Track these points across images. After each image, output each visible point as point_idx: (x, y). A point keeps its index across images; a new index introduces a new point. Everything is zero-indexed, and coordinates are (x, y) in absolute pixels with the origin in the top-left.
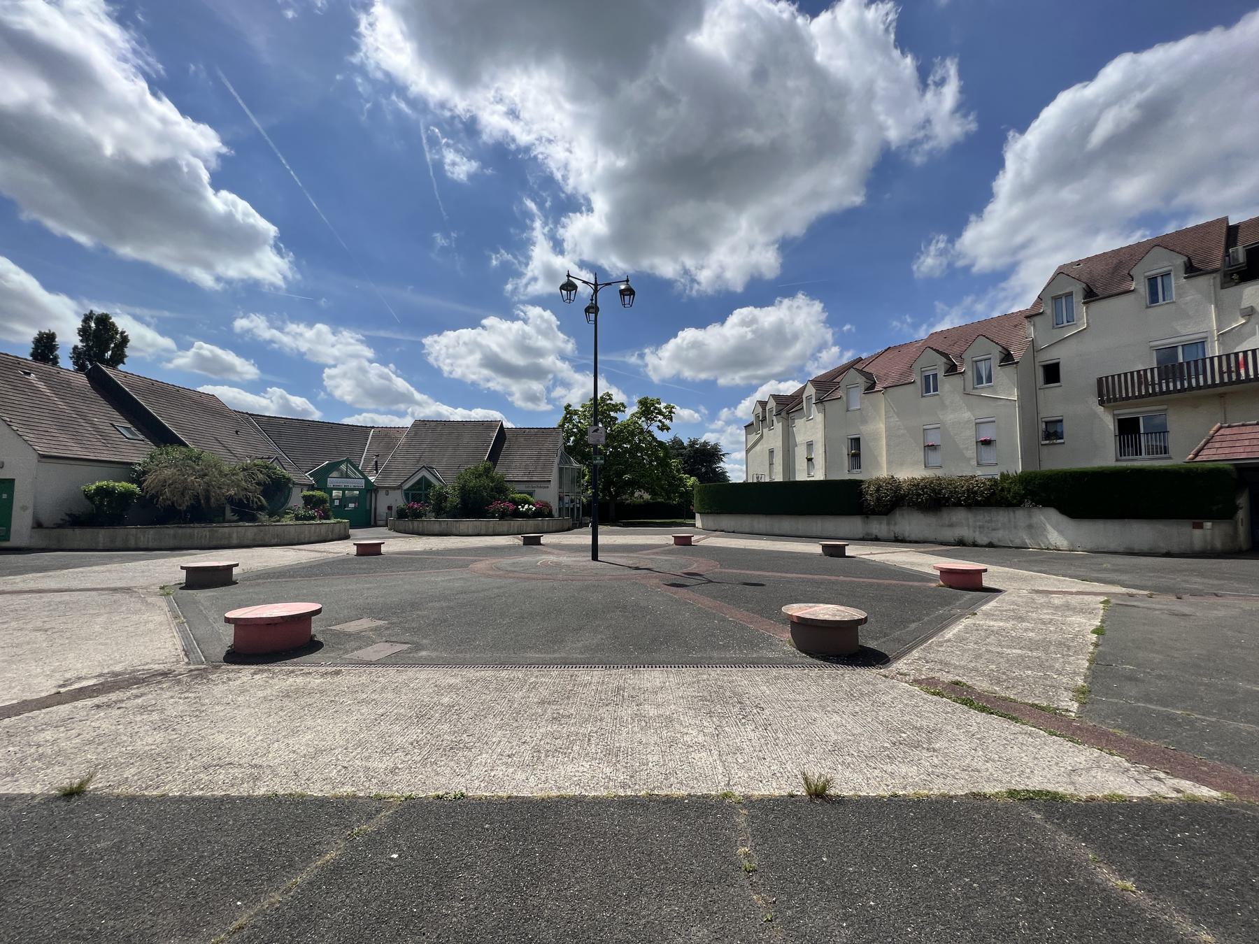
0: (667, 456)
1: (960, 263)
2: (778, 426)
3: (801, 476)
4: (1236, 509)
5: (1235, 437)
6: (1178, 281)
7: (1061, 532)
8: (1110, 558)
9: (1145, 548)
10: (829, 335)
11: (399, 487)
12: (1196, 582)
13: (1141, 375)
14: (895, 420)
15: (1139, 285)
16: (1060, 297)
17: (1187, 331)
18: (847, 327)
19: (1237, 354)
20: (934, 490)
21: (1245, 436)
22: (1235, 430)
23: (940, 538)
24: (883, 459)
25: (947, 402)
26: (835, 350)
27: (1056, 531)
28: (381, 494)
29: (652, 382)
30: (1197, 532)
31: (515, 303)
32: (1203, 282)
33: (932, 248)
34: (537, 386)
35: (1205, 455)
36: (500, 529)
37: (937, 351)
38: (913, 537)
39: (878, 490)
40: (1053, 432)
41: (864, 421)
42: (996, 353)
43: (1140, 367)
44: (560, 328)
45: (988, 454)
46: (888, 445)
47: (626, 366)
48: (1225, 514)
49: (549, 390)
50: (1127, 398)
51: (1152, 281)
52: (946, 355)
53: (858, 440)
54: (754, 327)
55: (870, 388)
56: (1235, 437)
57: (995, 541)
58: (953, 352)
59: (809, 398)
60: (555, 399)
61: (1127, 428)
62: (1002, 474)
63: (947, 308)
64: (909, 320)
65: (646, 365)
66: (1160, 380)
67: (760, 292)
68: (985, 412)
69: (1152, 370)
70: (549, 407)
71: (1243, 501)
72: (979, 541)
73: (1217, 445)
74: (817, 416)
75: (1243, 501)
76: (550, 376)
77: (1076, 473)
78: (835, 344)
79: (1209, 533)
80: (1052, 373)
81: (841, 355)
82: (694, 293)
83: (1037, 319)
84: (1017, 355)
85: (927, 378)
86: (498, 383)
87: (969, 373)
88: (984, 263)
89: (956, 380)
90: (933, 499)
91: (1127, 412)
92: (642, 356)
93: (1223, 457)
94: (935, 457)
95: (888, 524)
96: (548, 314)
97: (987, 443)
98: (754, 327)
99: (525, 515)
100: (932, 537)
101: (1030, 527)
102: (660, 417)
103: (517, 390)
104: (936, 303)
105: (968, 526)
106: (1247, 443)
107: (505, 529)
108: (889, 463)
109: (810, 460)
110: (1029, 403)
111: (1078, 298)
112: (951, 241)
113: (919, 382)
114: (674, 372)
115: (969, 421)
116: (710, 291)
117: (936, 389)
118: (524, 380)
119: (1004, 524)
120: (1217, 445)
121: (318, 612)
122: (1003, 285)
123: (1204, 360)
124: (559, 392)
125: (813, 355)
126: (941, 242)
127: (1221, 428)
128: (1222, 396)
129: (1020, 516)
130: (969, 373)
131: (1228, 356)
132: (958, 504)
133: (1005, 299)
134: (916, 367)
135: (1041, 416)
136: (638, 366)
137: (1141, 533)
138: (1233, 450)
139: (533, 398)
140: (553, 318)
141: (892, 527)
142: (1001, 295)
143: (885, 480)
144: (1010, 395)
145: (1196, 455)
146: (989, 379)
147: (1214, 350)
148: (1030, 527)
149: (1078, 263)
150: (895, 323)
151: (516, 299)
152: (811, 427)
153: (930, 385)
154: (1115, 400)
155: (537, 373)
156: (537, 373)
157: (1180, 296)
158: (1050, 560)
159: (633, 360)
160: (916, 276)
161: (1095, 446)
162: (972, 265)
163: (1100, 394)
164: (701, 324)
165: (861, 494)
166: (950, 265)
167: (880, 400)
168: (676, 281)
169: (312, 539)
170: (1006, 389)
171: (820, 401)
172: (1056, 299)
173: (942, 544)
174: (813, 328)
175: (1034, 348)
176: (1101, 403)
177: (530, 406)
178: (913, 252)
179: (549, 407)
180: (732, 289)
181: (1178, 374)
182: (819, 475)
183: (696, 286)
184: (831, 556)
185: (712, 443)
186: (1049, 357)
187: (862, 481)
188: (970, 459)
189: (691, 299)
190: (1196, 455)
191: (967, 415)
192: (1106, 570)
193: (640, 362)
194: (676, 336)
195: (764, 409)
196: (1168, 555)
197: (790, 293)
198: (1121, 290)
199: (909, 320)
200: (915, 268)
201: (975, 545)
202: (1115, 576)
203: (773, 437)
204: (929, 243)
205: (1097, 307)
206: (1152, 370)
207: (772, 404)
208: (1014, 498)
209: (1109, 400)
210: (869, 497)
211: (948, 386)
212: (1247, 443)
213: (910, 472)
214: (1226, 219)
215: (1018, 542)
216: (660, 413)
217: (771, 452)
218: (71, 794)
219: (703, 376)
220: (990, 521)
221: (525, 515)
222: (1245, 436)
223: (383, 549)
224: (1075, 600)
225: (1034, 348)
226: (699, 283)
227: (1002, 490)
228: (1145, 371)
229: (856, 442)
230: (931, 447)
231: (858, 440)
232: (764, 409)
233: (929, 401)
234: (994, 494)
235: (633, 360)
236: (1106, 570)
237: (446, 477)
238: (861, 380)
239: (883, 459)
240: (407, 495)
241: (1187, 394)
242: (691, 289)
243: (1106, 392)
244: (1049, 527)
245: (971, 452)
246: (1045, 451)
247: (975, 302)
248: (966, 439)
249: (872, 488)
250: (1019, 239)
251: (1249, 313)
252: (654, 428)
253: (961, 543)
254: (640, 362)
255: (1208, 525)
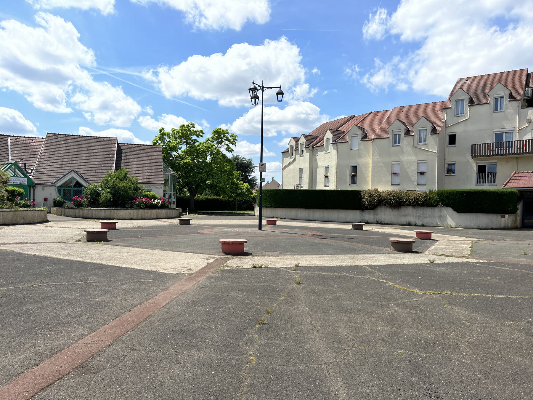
0: (232, 169)
1: (394, 31)
2: (307, 155)
3: (320, 186)
4: (517, 209)
5: (520, 178)
6: (506, 101)
7: (453, 219)
8: (471, 230)
9: (484, 227)
10: (302, 74)
11: (53, 185)
12: (499, 237)
13: (489, 145)
14: (377, 157)
15: (490, 100)
16: (459, 100)
17: (507, 126)
18: (315, 71)
19: (523, 141)
20: (398, 198)
21: (523, 178)
22: (520, 175)
23: (399, 222)
24: (370, 179)
25: (405, 150)
26: (306, 86)
27: (450, 217)
28: (38, 189)
29: (165, 97)
30: (503, 219)
31: (36, 11)
32: (516, 104)
33: (377, 17)
34: (57, 91)
35: (510, 185)
36: (145, 216)
37: (400, 121)
38: (386, 222)
39: (370, 196)
40: (450, 170)
41: (360, 156)
42: (429, 129)
43: (489, 142)
44: (80, 40)
45: (422, 178)
46: (372, 171)
47: (141, 80)
48: (513, 212)
49: (68, 95)
50: (483, 156)
51: (496, 99)
52: (404, 123)
53: (356, 167)
54: (248, 60)
55: (364, 138)
56: (520, 178)
57: (425, 224)
58: (408, 121)
59: (328, 140)
60: (75, 104)
61: (481, 169)
62: (430, 191)
63: (381, 64)
64: (357, 69)
65: (160, 82)
66: (496, 148)
67: (253, 33)
68: (422, 157)
69: (493, 143)
70: (69, 110)
71: (520, 206)
72: (418, 224)
73: (513, 181)
74: (333, 151)
75: (520, 206)
76: (70, 82)
77: (461, 191)
78: (306, 82)
79: (507, 220)
80: (452, 139)
81: (310, 91)
82: (202, 26)
83: (448, 110)
84: (439, 130)
85: (395, 135)
86: (17, 84)
87: (416, 136)
88: (407, 35)
89: (409, 139)
90: (397, 202)
91: (482, 162)
92: (156, 74)
93: (515, 186)
94: (397, 180)
95: (374, 214)
96: (69, 26)
97: (422, 173)
98: (248, 60)
99: (155, 207)
100: (395, 222)
101: (440, 216)
102: (227, 142)
103: (37, 93)
104: (375, 59)
105: (413, 216)
106: (523, 180)
107: (149, 216)
108: (373, 181)
109: (326, 177)
110: (442, 154)
111: (466, 103)
112: (390, 14)
113: (391, 138)
114: (183, 90)
115: (415, 161)
116: (215, 27)
117: (399, 143)
118: (43, 83)
119: (430, 215)
120: (513, 181)
121: (246, 242)
122: (418, 52)
123: (512, 142)
124: (78, 97)
125: (290, 88)
126: (382, 13)
127: (515, 173)
128: (517, 158)
129: (436, 211)
130: (416, 136)
131: (520, 141)
132: (409, 205)
133: (418, 61)
134: (390, 129)
135: (446, 161)
136: (153, 82)
137: (483, 219)
138: (519, 183)
139: (53, 101)
140: (75, 31)
141: (376, 216)
142: (417, 58)
143: (373, 191)
144: (434, 149)
145: (506, 185)
146: (425, 141)
147: (516, 138)
148: (440, 216)
149: (467, 79)
150: (348, 70)
151: (37, 6)
152: (328, 157)
153: (396, 141)
154: (478, 156)
155: (57, 78)
156: (57, 78)
157: (506, 109)
158: (449, 230)
159: (148, 75)
160: (364, 36)
161: (467, 181)
162: (401, 34)
163: (472, 153)
164: (207, 53)
165: (361, 198)
166: (387, 31)
167: (370, 145)
168: (187, 12)
169: (126, 217)
170: (433, 146)
171: (335, 142)
172: (457, 101)
173: (400, 225)
174: (291, 67)
175: (446, 126)
176: (472, 157)
177: (50, 108)
178: (363, 19)
179: (69, 110)
180: (232, 27)
181: (502, 147)
182: (332, 186)
183: (203, 19)
184: (357, 229)
185: (247, 159)
186: (452, 131)
187: (361, 191)
188: (414, 181)
189: (199, 30)
190: (506, 185)
191: (414, 158)
192: (470, 234)
193: (154, 79)
194: (185, 59)
195: (297, 143)
196: (492, 229)
197: (275, 37)
198: (484, 102)
199: (357, 69)
200: (364, 31)
201: (416, 225)
202: (474, 236)
203: (303, 161)
204: (375, 13)
205: (474, 108)
206: (493, 143)
207: (303, 140)
208: (434, 202)
209: (475, 156)
210: (365, 200)
211: (406, 141)
212: (523, 180)
213: (385, 187)
214: (527, 69)
215: (435, 224)
216: (227, 139)
217: (301, 170)
218: (297, 266)
219: (208, 96)
220: (423, 214)
221: (155, 207)
222: (523, 178)
223: (191, 222)
224: (462, 242)
225: (446, 126)
226: (206, 18)
227: (430, 198)
228: (490, 144)
229: (355, 168)
230: (396, 174)
231: (356, 167)
232: (297, 143)
233: (395, 149)
234: (426, 200)
235: (148, 75)
236: (470, 234)
237: (97, 177)
238: (360, 133)
239: (370, 179)
240: (59, 190)
241: (505, 157)
242: (200, 23)
243: (475, 152)
244: (448, 216)
245: (414, 178)
246: (446, 178)
247: (400, 61)
248: (413, 170)
249: (367, 195)
250: (430, 20)
251: (529, 122)
252: (223, 150)
253: (409, 224)
254: (154, 79)
255: (507, 216)
